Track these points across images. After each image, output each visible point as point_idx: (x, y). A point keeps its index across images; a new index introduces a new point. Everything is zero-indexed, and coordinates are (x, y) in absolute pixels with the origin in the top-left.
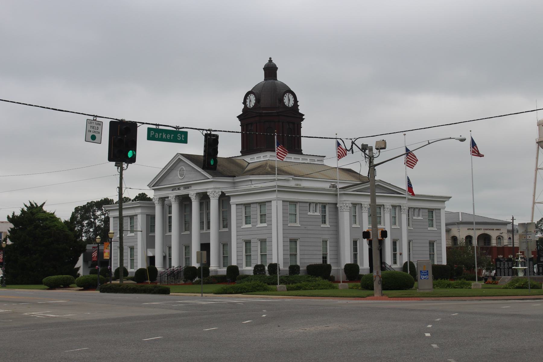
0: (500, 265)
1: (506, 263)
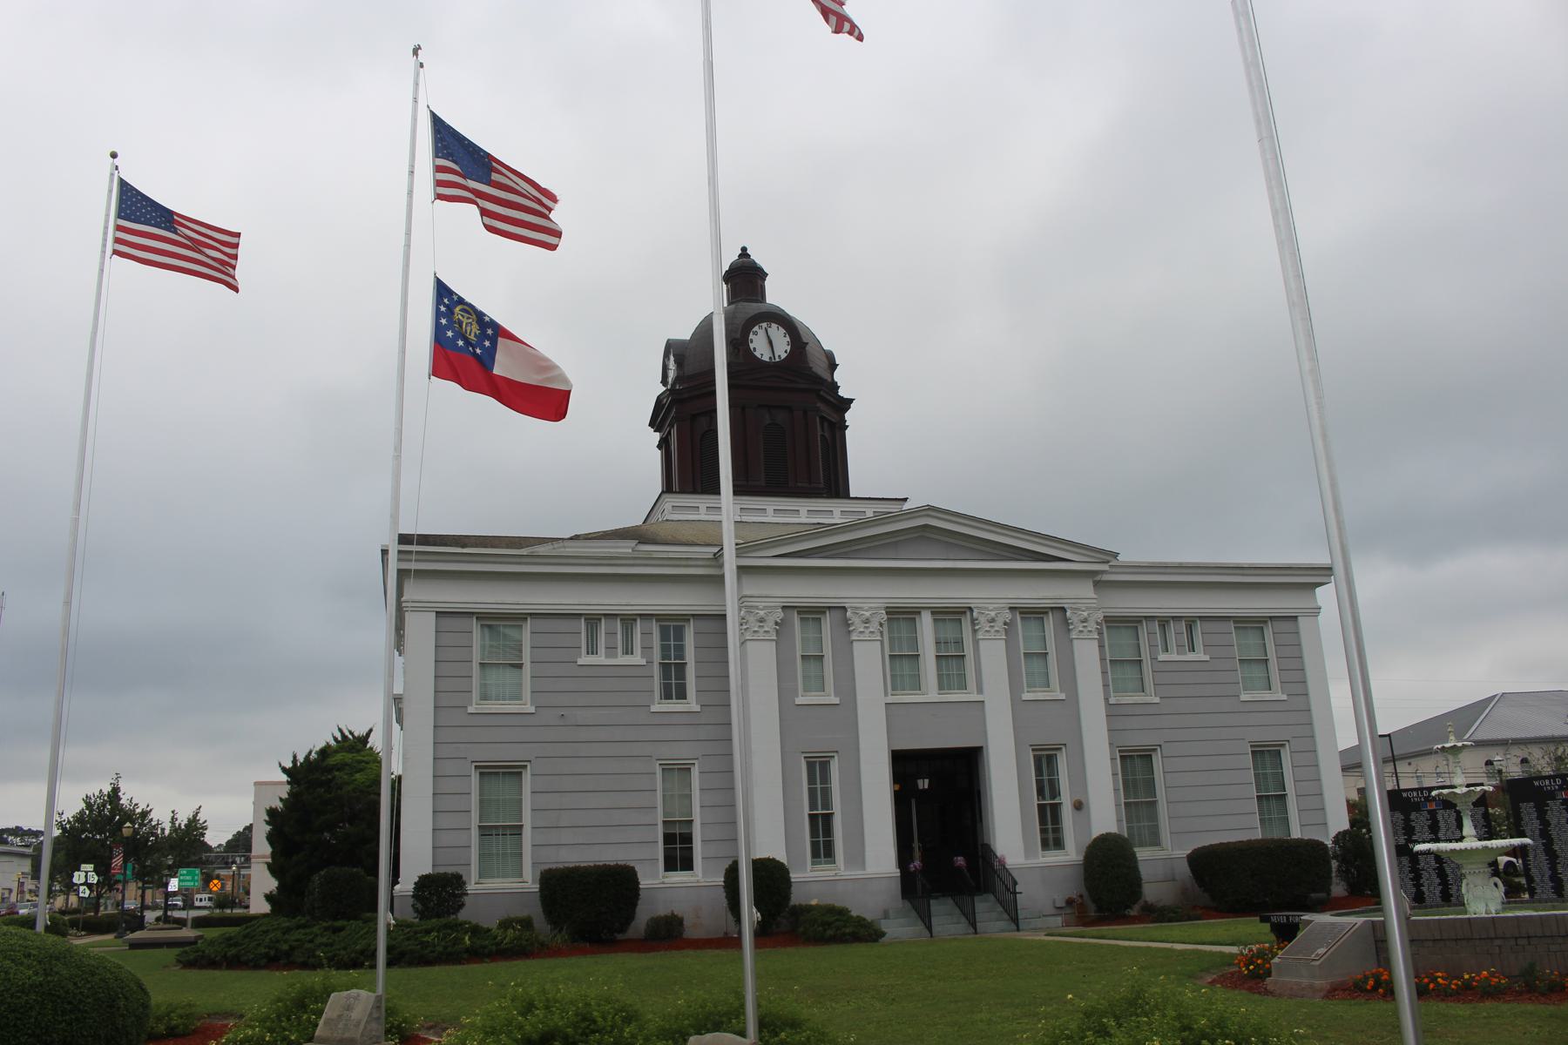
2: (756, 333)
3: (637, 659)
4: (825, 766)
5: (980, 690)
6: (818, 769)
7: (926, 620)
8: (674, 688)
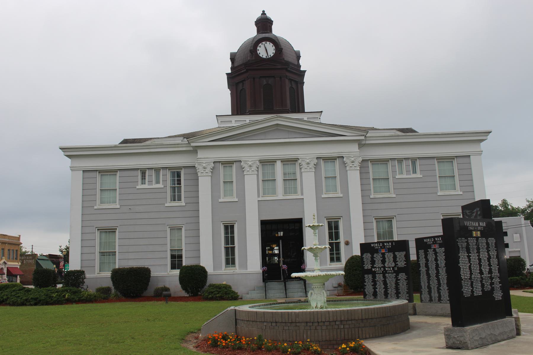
0: (373, 262)
1: (389, 256)
2: (260, 47)
3: (161, 185)
4: (232, 227)
5: (302, 194)
6: (229, 229)
7: (279, 164)
8: (177, 197)
